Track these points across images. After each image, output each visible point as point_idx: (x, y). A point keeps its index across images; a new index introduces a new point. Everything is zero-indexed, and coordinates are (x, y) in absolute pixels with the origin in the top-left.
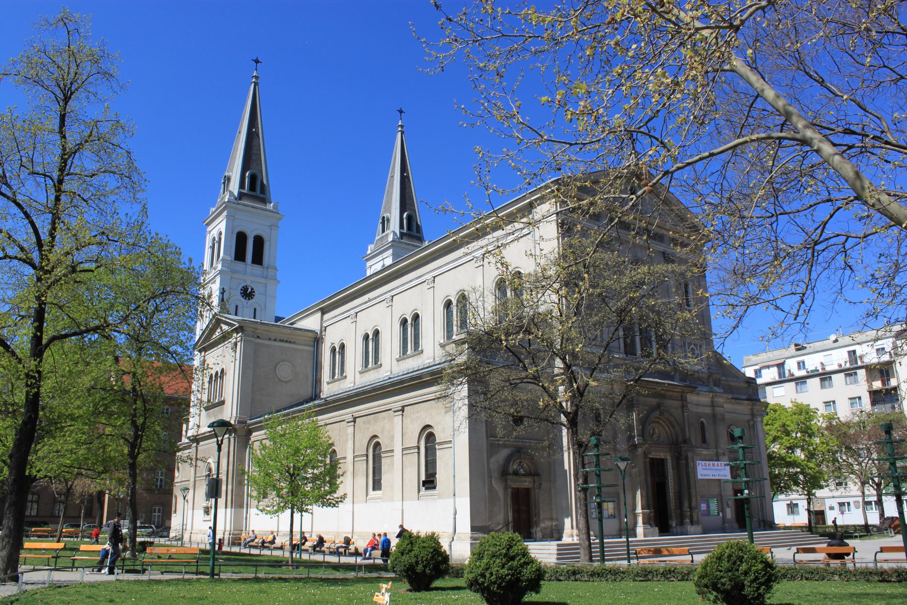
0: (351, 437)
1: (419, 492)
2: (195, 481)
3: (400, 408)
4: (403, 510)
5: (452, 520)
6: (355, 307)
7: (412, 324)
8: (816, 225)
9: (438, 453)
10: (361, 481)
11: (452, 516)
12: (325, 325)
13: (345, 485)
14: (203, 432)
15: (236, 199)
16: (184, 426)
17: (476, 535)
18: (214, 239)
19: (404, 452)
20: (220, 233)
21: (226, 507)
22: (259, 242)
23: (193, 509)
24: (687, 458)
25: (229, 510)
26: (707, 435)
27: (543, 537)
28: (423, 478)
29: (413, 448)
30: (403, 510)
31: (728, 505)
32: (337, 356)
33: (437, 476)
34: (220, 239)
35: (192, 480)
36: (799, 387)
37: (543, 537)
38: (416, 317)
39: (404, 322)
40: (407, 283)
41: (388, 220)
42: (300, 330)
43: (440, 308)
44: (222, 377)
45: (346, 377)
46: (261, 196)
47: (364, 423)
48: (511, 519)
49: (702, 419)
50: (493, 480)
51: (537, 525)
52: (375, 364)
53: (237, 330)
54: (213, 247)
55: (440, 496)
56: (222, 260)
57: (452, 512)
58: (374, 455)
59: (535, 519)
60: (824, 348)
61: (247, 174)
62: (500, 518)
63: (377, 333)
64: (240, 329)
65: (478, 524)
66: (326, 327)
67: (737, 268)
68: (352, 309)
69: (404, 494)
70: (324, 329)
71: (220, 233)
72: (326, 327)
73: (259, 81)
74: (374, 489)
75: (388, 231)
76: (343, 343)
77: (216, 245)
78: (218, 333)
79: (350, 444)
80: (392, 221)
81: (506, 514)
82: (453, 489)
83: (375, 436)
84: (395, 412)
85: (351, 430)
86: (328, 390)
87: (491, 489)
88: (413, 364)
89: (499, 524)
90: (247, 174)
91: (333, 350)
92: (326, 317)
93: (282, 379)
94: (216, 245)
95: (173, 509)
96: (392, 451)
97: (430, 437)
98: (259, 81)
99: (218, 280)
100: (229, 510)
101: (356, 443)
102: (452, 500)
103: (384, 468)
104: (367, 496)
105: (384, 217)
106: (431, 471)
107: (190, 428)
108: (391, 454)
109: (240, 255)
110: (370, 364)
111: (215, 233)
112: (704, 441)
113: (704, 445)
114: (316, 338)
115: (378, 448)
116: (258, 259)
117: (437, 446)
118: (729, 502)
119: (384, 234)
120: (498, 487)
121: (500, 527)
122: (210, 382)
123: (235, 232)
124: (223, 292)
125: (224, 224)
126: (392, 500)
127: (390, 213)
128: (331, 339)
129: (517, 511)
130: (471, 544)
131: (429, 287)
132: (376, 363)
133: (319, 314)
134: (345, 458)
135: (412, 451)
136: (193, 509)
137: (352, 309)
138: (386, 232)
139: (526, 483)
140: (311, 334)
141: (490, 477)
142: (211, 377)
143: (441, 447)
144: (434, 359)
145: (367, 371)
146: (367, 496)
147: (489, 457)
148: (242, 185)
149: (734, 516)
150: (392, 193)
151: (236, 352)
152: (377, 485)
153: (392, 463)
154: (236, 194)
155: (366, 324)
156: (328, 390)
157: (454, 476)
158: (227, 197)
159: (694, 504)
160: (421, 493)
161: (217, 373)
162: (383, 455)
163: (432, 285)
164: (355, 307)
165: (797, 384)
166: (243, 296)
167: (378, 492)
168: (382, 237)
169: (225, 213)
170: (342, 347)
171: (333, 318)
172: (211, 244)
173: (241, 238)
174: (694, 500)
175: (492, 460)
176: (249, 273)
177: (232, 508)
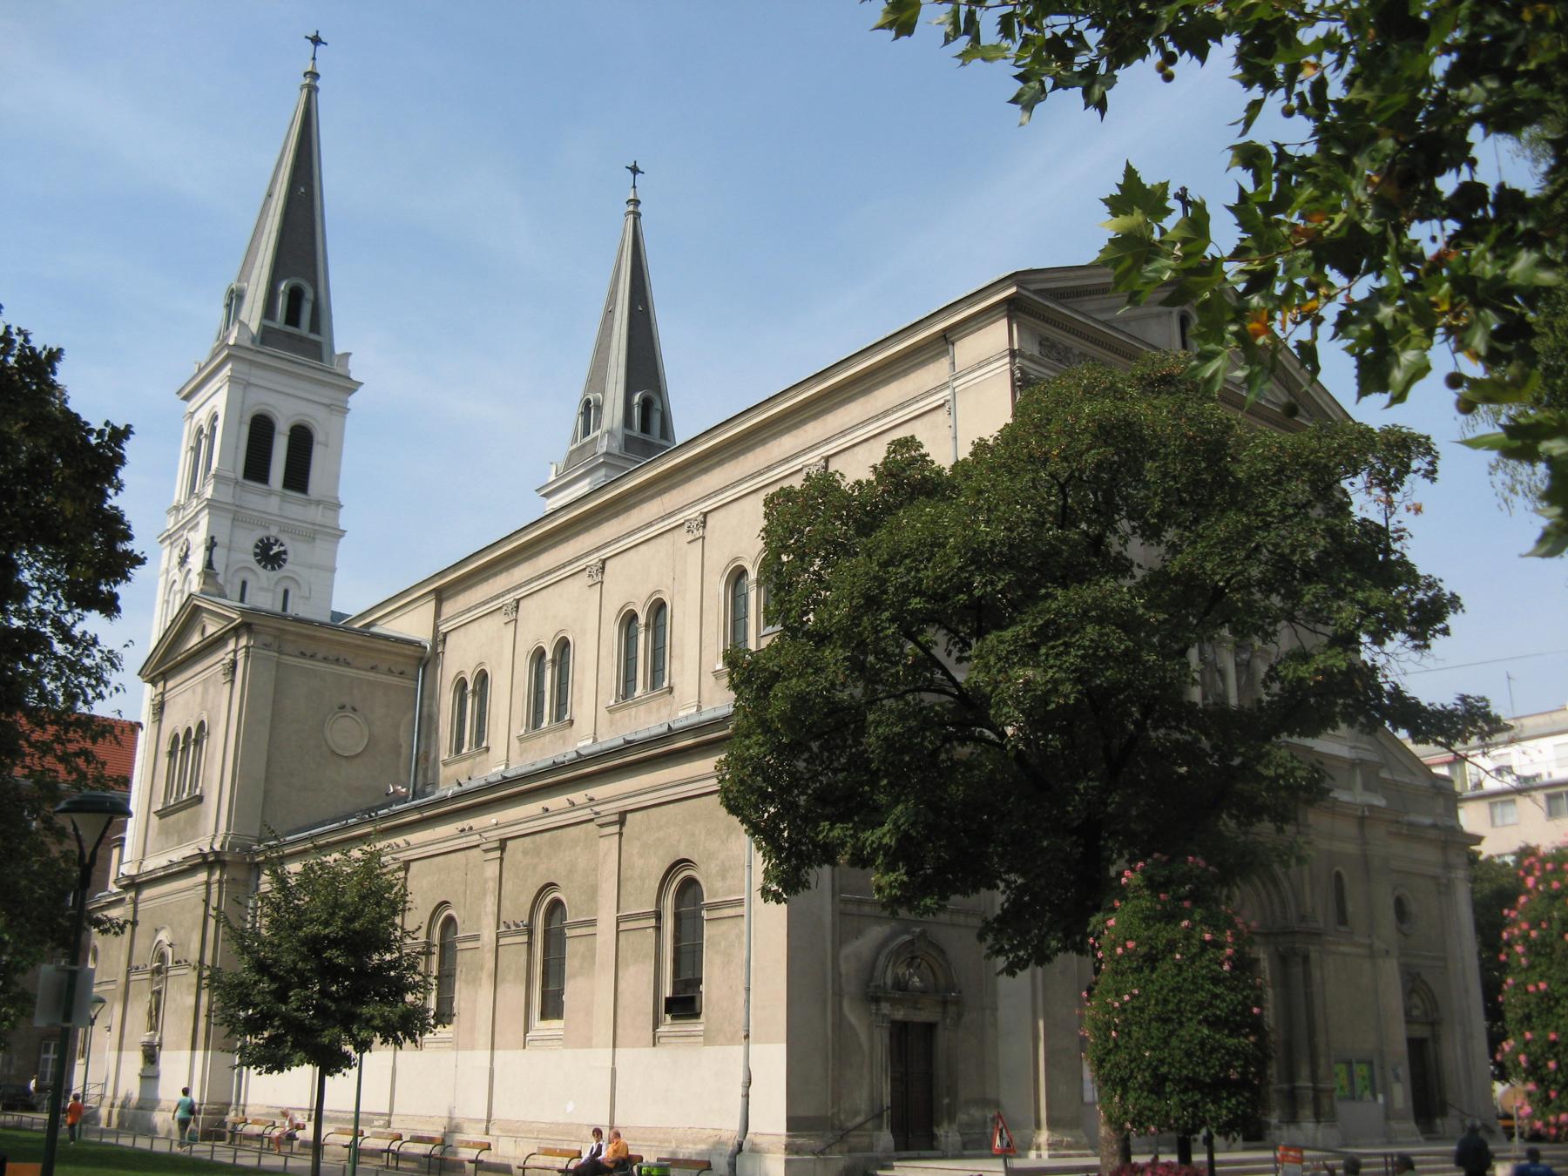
0: (492, 885)
1: (656, 1025)
2: (128, 983)
3: (616, 818)
4: (614, 1071)
5: (739, 1100)
6: (515, 588)
7: (647, 625)
9: (708, 931)
10: (513, 993)
11: (740, 1091)
12: (443, 629)
13: (472, 998)
14: (150, 868)
15: (253, 340)
16: (116, 852)
17: (799, 1141)
18: (200, 431)
20: (215, 418)
21: (193, 1048)
22: (302, 440)
23: (120, 1049)
24: (1306, 959)
25: (199, 1054)
27: (965, 1146)
28: (667, 991)
29: (645, 916)
30: (614, 1071)
31: (1397, 1077)
32: (470, 697)
33: (703, 988)
34: (213, 429)
35: (122, 979)
36: (1498, 811)
37: (965, 1146)
38: (658, 608)
39: (629, 619)
40: (639, 529)
41: (599, 408)
42: (386, 638)
43: (717, 587)
44: (198, 742)
45: (488, 749)
46: (313, 337)
47: (525, 853)
48: (887, 1101)
49: (1337, 868)
52: (558, 720)
53: (236, 631)
54: (196, 450)
55: (709, 1039)
56: (215, 476)
58: (546, 932)
59: (946, 1101)
60: (1556, 729)
61: (282, 288)
63: (563, 646)
64: (244, 627)
66: (445, 635)
68: (509, 591)
69: (619, 1031)
70: (440, 639)
71: (215, 418)
72: (445, 635)
73: (318, 84)
74: (544, 1016)
75: (598, 433)
76: (483, 670)
77: (204, 443)
78: (195, 640)
80: (607, 410)
82: (743, 1021)
83: (550, 886)
85: (492, 870)
86: (452, 777)
87: (840, 1023)
88: (646, 721)
89: (856, 1113)
90: (282, 288)
91: (461, 685)
92: (449, 608)
93: (338, 752)
94: (204, 443)
95: (79, 1045)
96: (592, 923)
98: (318, 84)
99: (204, 520)
100: (199, 1054)
101: (506, 904)
102: (739, 1050)
103: (571, 965)
104: (526, 1031)
105: (588, 402)
106: (687, 975)
107: (125, 859)
109: (256, 468)
110: (546, 719)
111: (202, 417)
112: (1342, 918)
113: (1342, 929)
114: (422, 659)
115: (558, 913)
116: (297, 478)
117: (704, 913)
119: (588, 439)
120: (854, 1016)
121: (859, 1119)
122: (172, 754)
123: (248, 419)
124: (211, 545)
125: (223, 395)
126: (587, 1043)
127: (603, 393)
128: (458, 660)
129: (901, 1082)
130: (787, 1162)
131: (690, 537)
132: (559, 718)
133: (431, 606)
134: (476, 938)
135: (643, 923)
136: (120, 1049)
137: (509, 591)
138: (592, 435)
140: (408, 650)
141: (839, 994)
143: (716, 914)
144: (699, 707)
145: (537, 736)
146: (526, 1031)
147: (840, 940)
148: (269, 310)
149: (1410, 1104)
150: (609, 348)
151: (232, 682)
152: (552, 1007)
153: (591, 955)
154: (254, 327)
155: (539, 627)
156: (452, 777)
157: (748, 990)
158: (234, 333)
159: (1322, 1072)
160: (661, 1029)
161: (189, 730)
162: (568, 933)
163: (699, 533)
164: (515, 588)
165: (1491, 805)
166: (259, 562)
167: (555, 1025)
168: (583, 446)
169: (227, 370)
170: (482, 678)
171: (463, 613)
172: (192, 443)
173: (261, 429)
174: (1322, 1061)
175: (847, 950)
176: (271, 500)
177: (206, 1048)
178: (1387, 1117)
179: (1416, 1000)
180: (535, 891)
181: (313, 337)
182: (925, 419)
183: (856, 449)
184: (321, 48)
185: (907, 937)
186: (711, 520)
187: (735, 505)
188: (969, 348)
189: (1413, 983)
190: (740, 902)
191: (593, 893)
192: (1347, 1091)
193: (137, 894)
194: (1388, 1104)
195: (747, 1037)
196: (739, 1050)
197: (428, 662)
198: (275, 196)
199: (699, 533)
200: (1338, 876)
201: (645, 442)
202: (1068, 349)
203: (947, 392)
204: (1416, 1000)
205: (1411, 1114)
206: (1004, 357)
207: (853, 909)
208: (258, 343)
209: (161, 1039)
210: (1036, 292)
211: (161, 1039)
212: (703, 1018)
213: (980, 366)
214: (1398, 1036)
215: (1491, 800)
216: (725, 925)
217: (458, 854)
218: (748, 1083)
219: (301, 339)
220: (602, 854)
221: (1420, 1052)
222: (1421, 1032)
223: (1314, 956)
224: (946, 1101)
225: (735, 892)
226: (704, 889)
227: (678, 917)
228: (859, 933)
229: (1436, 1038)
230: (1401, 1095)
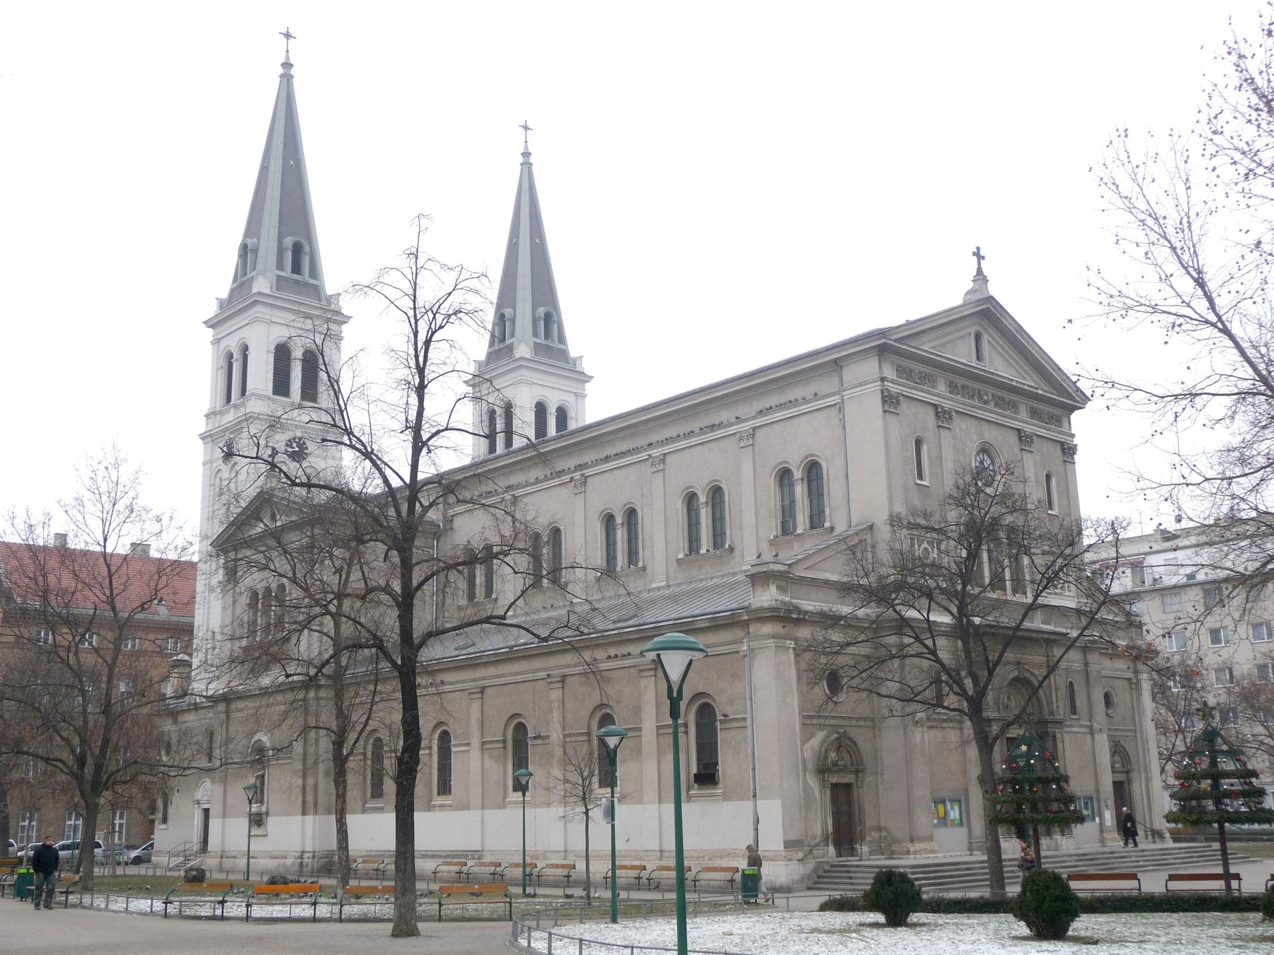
4: (660, 817)
5: (752, 832)
8: (1206, 317)
9: (721, 736)
11: (751, 827)
19: (660, 732)
24: (1054, 737)
26: (1078, 703)
31: (1107, 806)
33: (720, 767)
38: (631, 514)
43: (679, 505)
48: (830, 829)
50: (807, 775)
51: (862, 839)
55: (726, 797)
57: (751, 820)
59: (859, 828)
62: (817, 829)
65: (792, 836)
67: (119, 776)
79: (556, 716)
81: (824, 822)
83: (516, 715)
84: (470, 693)
85: (476, 707)
96: (639, 729)
97: (521, 728)
108: (636, 734)
112: (1074, 710)
118: (1109, 802)
120: (813, 782)
121: (817, 840)
123: (272, 348)
129: (837, 816)
131: (654, 469)
135: (580, 738)
139: (847, 779)
142: (254, 595)
147: (804, 741)
162: (453, 749)
175: (808, 745)
178: (1102, 831)
179: (1117, 758)
180: (592, 708)
181: (312, 281)
182: (822, 412)
183: (774, 426)
184: (291, 40)
185: (836, 735)
186: (668, 460)
187: (687, 451)
188: (853, 373)
189: (1118, 750)
190: (744, 719)
191: (637, 711)
192: (959, 822)
193: (228, 706)
194: (1102, 824)
195: (755, 796)
196: (748, 805)
197: (440, 536)
198: (272, 168)
199: (662, 466)
200: (1071, 683)
201: (548, 347)
202: (911, 371)
203: (837, 397)
204: (1117, 758)
205: (1116, 830)
206: (876, 381)
207: (808, 721)
208: (274, 290)
209: (268, 809)
210: (896, 340)
211: (268, 809)
212: (720, 785)
213: (860, 385)
214: (1107, 780)
215: (1162, 592)
216: (733, 733)
217: (526, 684)
218: (757, 822)
219: (305, 284)
220: (643, 688)
221: (1121, 791)
222: (1120, 777)
223: (1058, 735)
224: (859, 828)
225: (740, 714)
226: (717, 710)
227: (698, 726)
228: (812, 735)
229: (1129, 781)
230: (1109, 817)
